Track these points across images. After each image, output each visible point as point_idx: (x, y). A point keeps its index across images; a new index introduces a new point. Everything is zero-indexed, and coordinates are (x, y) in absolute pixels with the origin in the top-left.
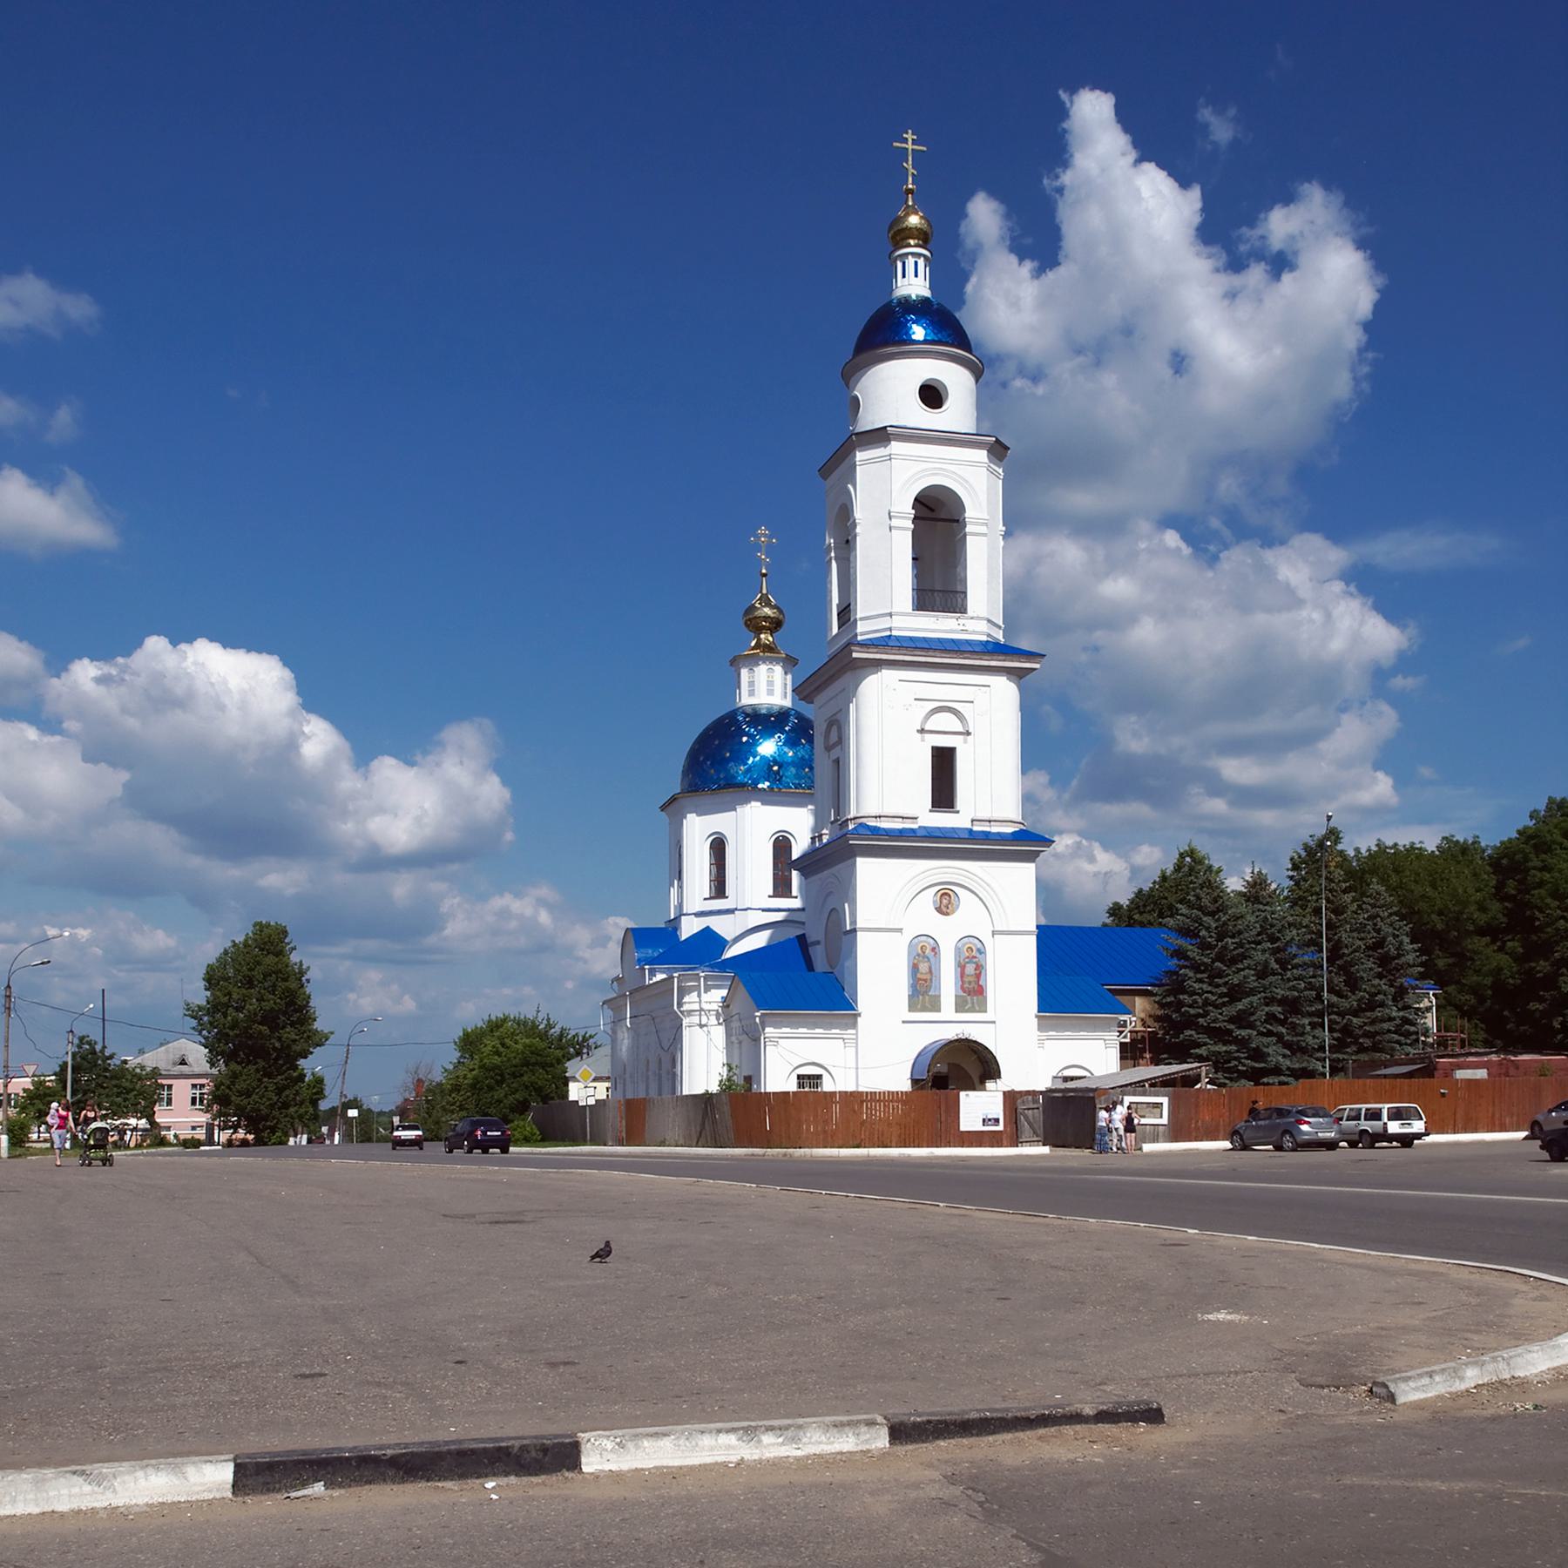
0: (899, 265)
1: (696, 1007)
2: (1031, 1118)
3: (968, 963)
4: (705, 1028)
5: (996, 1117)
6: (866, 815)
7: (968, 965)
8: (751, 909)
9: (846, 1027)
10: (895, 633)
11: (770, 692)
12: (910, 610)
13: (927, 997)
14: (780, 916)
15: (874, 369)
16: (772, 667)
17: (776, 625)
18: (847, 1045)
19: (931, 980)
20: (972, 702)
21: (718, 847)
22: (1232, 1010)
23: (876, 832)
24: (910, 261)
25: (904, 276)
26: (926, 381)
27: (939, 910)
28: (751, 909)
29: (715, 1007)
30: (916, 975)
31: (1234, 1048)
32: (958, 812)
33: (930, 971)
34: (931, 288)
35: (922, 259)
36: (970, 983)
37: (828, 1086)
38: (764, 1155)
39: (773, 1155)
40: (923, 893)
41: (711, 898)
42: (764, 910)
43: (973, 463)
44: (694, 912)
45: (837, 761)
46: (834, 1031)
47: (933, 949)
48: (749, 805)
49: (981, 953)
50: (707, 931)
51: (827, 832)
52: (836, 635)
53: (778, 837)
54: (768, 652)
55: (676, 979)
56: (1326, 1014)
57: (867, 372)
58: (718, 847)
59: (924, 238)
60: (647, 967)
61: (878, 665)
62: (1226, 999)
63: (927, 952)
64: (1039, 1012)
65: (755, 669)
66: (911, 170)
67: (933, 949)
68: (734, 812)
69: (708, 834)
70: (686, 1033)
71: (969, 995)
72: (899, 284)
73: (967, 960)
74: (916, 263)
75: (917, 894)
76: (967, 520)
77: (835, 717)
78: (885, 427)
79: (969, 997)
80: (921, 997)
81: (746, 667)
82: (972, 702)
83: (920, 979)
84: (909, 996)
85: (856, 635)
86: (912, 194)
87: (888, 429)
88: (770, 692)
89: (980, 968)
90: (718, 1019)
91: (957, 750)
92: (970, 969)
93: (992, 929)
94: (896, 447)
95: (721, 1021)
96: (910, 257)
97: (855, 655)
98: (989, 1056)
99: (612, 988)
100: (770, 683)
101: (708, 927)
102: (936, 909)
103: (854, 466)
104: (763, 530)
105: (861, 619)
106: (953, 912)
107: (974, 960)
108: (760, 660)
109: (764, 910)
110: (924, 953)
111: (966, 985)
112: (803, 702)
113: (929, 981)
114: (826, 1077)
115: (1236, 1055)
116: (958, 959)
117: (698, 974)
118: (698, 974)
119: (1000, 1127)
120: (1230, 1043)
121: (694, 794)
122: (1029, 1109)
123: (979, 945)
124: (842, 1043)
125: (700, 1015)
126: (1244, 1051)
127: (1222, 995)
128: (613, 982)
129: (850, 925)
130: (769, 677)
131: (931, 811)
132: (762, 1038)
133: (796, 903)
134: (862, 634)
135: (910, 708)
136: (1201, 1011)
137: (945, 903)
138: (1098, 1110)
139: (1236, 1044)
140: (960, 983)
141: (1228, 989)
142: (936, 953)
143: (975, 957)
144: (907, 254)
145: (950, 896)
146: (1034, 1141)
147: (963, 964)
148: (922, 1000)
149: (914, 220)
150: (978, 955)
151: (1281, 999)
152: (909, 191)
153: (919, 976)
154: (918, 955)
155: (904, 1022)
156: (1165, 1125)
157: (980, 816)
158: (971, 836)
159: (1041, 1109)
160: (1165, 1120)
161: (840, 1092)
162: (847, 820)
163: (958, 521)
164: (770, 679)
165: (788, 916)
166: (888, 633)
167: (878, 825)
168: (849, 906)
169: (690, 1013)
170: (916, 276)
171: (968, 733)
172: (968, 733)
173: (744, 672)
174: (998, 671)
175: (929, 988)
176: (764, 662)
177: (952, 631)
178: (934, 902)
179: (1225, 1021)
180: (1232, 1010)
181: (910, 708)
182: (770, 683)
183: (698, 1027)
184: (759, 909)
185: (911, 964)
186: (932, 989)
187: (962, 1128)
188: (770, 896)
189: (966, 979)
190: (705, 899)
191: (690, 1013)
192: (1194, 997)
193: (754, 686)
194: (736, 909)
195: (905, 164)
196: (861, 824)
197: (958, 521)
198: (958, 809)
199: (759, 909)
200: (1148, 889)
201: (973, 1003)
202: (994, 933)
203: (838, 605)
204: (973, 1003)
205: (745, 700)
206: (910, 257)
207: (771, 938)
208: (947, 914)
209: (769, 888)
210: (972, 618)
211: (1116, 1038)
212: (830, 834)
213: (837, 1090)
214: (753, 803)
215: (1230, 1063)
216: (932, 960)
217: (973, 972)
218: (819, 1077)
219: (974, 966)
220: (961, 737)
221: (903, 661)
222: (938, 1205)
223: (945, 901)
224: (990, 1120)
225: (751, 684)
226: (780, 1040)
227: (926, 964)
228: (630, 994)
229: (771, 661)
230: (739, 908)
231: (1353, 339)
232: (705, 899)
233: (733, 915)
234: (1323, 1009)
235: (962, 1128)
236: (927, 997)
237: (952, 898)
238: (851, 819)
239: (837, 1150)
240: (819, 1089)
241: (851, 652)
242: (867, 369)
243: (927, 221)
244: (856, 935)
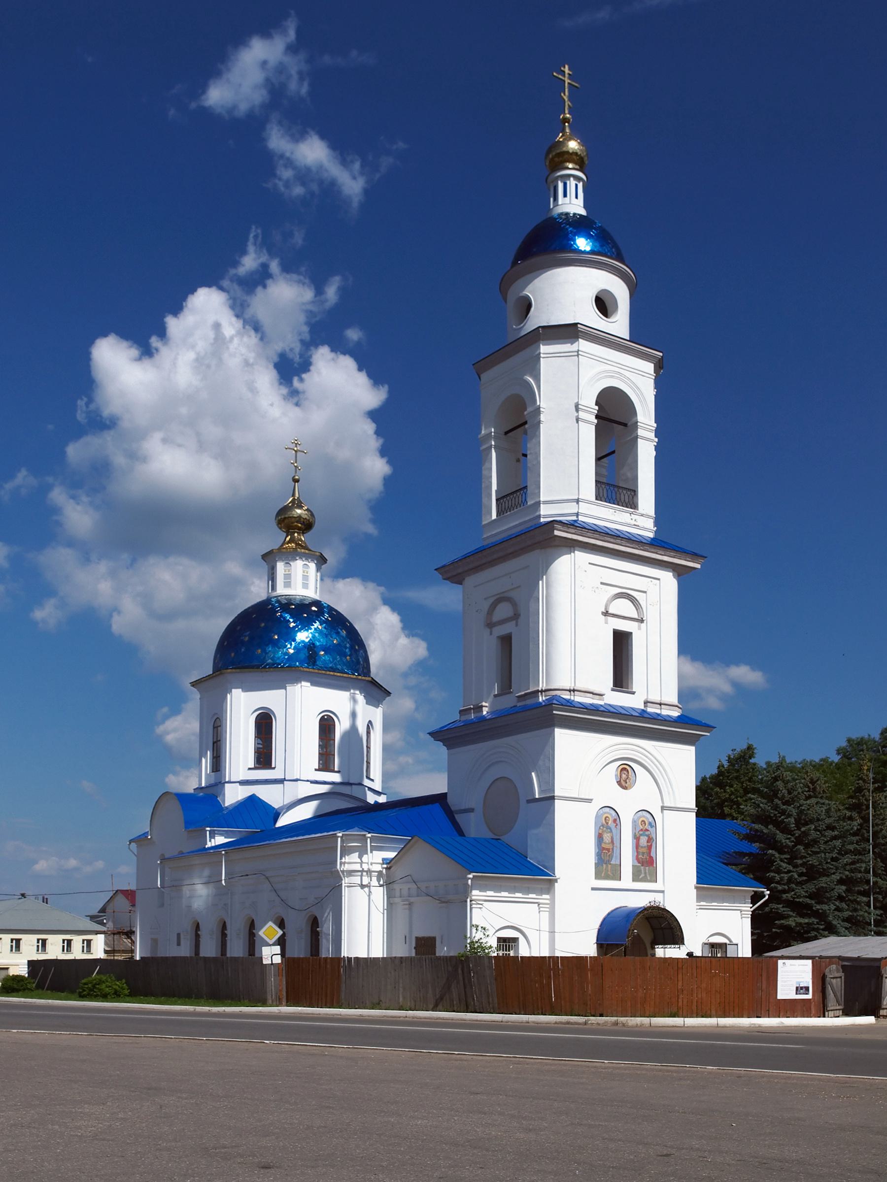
0: (560, 186)
1: (357, 867)
2: (835, 985)
3: (641, 835)
4: (366, 889)
5: (806, 985)
6: (561, 688)
7: (641, 837)
8: (300, 780)
9: (541, 892)
11: (305, 586)
12: (593, 498)
13: (609, 866)
14: (324, 789)
15: (549, 273)
16: (307, 563)
18: (541, 909)
19: (613, 849)
22: (811, 887)
23: (569, 705)
24: (572, 183)
25: (565, 195)
27: (619, 783)
28: (300, 780)
29: (378, 868)
30: (601, 845)
31: (815, 921)
32: (633, 693)
33: (612, 842)
34: (585, 207)
35: (581, 183)
36: (643, 853)
37: (524, 951)
38: (586, 1023)
39: (598, 1024)
41: (255, 768)
42: (312, 782)
43: (642, 374)
44: (238, 780)
45: (506, 641)
46: (531, 896)
47: (615, 821)
48: (299, 685)
49: (652, 827)
50: (253, 800)
51: (487, 704)
52: (495, 520)
53: (323, 716)
55: (339, 839)
56: (872, 894)
57: (547, 271)
59: (580, 162)
60: (208, 829)
61: (571, 545)
62: (805, 878)
63: (610, 823)
64: (697, 883)
65: (291, 563)
66: (566, 98)
68: (283, 691)
70: (345, 892)
71: (642, 866)
72: (560, 202)
74: (576, 185)
75: (606, 766)
76: (639, 424)
80: (604, 866)
81: (283, 561)
83: (604, 849)
84: (595, 863)
85: (539, 516)
86: (568, 123)
87: (579, 326)
88: (305, 586)
89: (651, 841)
90: (379, 881)
92: (643, 841)
93: (661, 805)
94: (583, 345)
95: (381, 883)
96: (572, 179)
97: (556, 533)
98: (675, 923)
99: (129, 848)
100: (305, 578)
101: (254, 794)
105: (546, 502)
106: (631, 788)
108: (297, 555)
109: (312, 782)
110: (607, 823)
111: (640, 856)
113: (611, 850)
114: (522, 941)
115: (816, 927)
116: (634, 831)
117: (365, 835)
118: (365, 835)
119: (809, 996)
120: (809, 916)
121: (238, 670)
122: (834, 978)
123: (651, 819)
125: (362, 876)
126: (823, 923)
127: (801, 875)
128: (130, 843)
129: (539, 794)
130: (304, 572)
131: (613, 690)
132: (468, 900)
133: (336, 778)
135: (596, 590)
136: (786, 887)
137: (625, 778)
138: (884, 978)
139: (815, 917)
140: (636, 854)
141: (806, 869)
143: (647, 830)
144: (569, 176)
145: (628, 771)
146: (836, 1010)
147: (638, 836)
149: (573, 145)
150: (650, 829)
151: (787, 882)
152: (565, 120)
153: (603, 845)
154: (603, 825)
158: (643, 715)
159: (843, 977)
161: (561, 957)
162: (538, 691)
163: (625, 425)
164: (305, 574)
165: (332, 789)
166: (574, 518)
167: (572, 698)
168: (537, 776)
169: (351, 873)
170: (577, 197)
171: (642, 621)
172: (642, 621)
173: (280, 566)
174: (667, 567)
175: (611, 857)
176: (301, 558)
177: (629, 525)
178: (616, 776)
179: (806, 897)
180: (811, 887)
181: (596, 590)
182: (305, 578)
183: (359, 888)
184: (308, 781)
185: (597, 834)
186: (614, 859)
187: (779, 997)
188: (316, 770)
189: (641, 850)
190: (250, 769)
191: (351, 873)
192: (782, 875)
193: (290, 578)
195: (562, 94)
196: (554, 697)
197: (625, 425)
198: (634, 690)
199: (308, 781)
203: (496, 491)
204: (645, 873)
206: (572, 179)
207: (318, 808)
208: (625, 788)
209: (314, 760)
210: (642, 515)
211: (749, 909)
212: (491, 707)
214: (304, 683)
215: (809, 933)
216: (614, 830)
217: (646, 844)
218: (515, 940)
219: (647, 838)
222: (604, 1062)
223: (624, 776)
224: (802, 988)
225: (288, 577)
226: (485, 904)
227: (609, 835)
228: (226, 853)
230: (301, 779)
231: (527, 407)
232: (250, 769)
234: (869, 889)
235: (779, 997)
236: (609, 866)
237: (630, 771)
238: (542, 691)
240: (512, 953)
241: (553, 529)
244: (554, 802)
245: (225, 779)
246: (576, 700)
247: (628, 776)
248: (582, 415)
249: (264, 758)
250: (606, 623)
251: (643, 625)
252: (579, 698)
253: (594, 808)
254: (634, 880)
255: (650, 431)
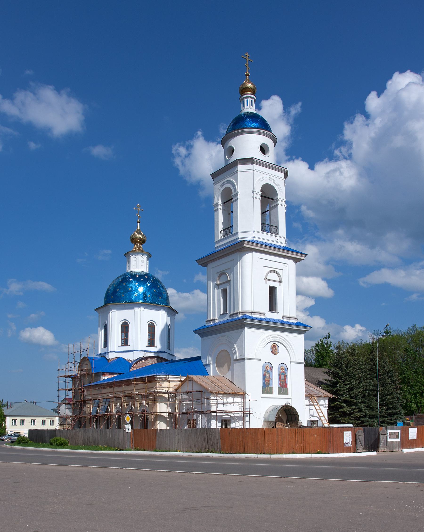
10: (255, 239)
13: (268, 388)
17: (143, 242)
19: (270, 380)
20: (282, 270)
21: (125, 327)
25: (247, 105)
26: (269, 152)
27: (272, 352)
30: (265, 379)
35: (254, 100)
36: (283, 382)
40: (268, 344)
43: (280, 178)
47: (271, 368)
49: (286, 371)
54: (140, 252)
58: (125, 327)
67: (271, 368)
69: (121, 320)
71: (282, 387)
73: (282, 373)
77: (223, 272)
78: (252, 158)
79: (282, 388)
82: (282, 270)
83: (266, 380)
89: (286, 376)
91: (277, 288)
92: (283, 377)
94: (255, 166)
102: (271, 351)
103: (237, 172)
104: (138, 205)
105: (241, 232)
107: (284, 373)
110: (267, 369)
112: (200, 266)
123: (286, 367)
124: (323, 407)
134: (241, 238)
137: (275, 350)
142: (271, 370)
148: (267, 388)
150: (285, 371)
152: (247, 75)
153: (266, 379)
155: (261, 398)
156: (399, 441)
157: (286, 315)
158: (282, 322)
159: (364, 435)
160: (399, 439)
166: (253, 239)
167: (252, 316)
170: (252, 106)
171: (281, 282)
175: (269, 384)
178: (271, 349)
188: (147, 346)
194: (134, 351)
200: (133, 360)
201: (284, 391)
202: (291, 362)
204: (284, 391)
205: (128, 270)
213: (259, 428)
217: (283, 378)
220: (278, 283)
221: (261, 250)
223: (274, 349)
227: (268, 374)
229: (143, 255)
233: (133, 353)
236: (268, 388)
239: (311, 455)
242: (233, 138)
243: (254, 85)
245: (109, 350)
246: (254, 316)
247: (276, 349)
248: (255, 195)
249: (125, 342)
250: (266, 283)
251: (282, 284)
252: (255, 316)
253: (261, 363)
254: (279, 394)
255: (283, 201)
